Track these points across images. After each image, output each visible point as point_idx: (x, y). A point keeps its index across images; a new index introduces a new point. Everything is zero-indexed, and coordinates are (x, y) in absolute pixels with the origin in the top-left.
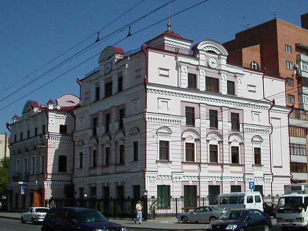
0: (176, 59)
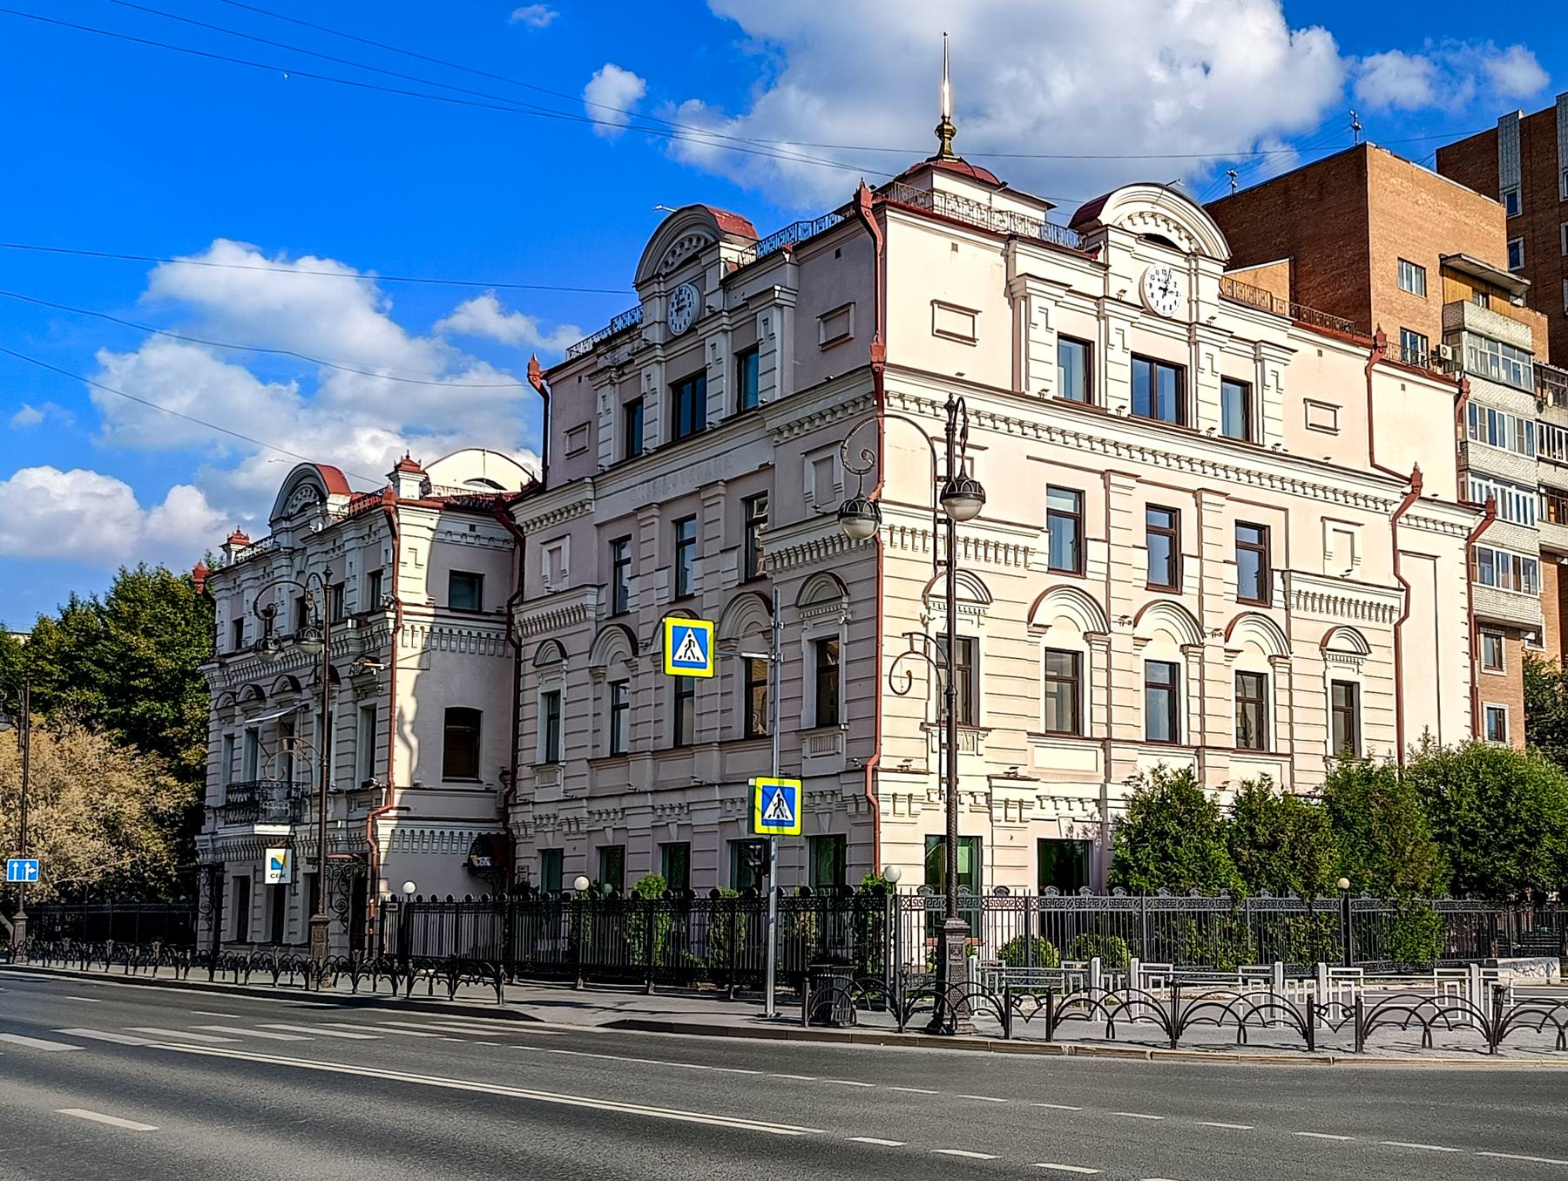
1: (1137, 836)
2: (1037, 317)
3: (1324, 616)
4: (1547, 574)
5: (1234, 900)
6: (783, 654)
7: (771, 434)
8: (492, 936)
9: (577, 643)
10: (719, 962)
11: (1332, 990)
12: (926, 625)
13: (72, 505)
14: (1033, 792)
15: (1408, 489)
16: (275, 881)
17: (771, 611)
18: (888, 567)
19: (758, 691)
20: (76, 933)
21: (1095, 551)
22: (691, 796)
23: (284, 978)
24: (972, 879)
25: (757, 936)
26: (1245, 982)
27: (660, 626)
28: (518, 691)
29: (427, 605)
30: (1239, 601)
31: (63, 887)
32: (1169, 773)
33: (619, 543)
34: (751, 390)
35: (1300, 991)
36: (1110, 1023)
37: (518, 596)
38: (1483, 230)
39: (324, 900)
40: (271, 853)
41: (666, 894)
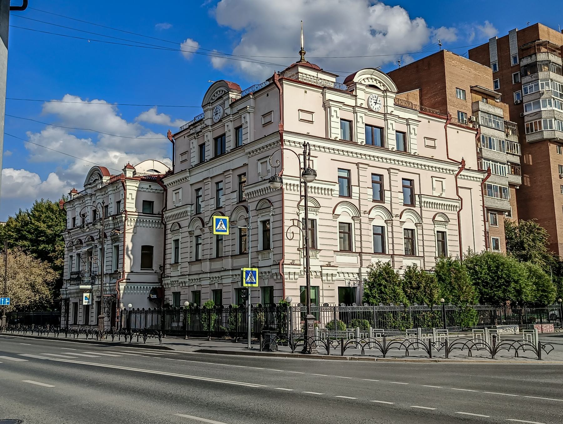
0: (323, 94)
1: (372, 286)
2: (333, 113)
3: (433, 210)
4: (512, 192)
5: (405, 307)
6: (251, 226)
7: (247, 154)
8: (158, 322)
9: (185, 223)
10: (232, 329)
11: (438, 337)
12: (298, 216)
13: (20, 181)
14: (336, 270)
15: (461, 166)
16: (86, 304)
17: (248, 212)
18: (286, 196)
19: (244, 238)
20: (22, 322)
21: (355, 190)
22: (222, 274)
23: (90, 336)
24: (316, 301)
25: (245, 320)
26: (408, 334)
27: (211, 218)
28: (165, 240)
29: (136, 212)
30: (405, 205)
31: (17, 307)
32: (381, 263)
33: (198, 190)
34: (240, 139)
35: (427, 337)
36: (363, 349)
37: (165, 208)
38: (485, 77)
39: (102, 310)
40: (85, 295)
41: (214, 307)
